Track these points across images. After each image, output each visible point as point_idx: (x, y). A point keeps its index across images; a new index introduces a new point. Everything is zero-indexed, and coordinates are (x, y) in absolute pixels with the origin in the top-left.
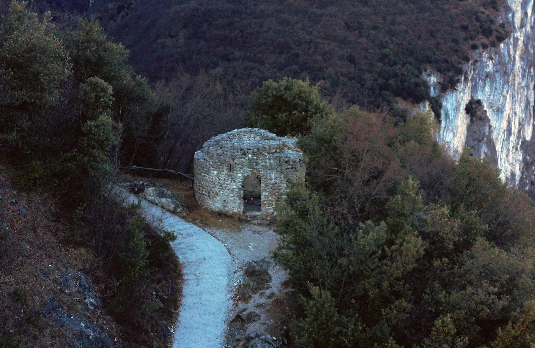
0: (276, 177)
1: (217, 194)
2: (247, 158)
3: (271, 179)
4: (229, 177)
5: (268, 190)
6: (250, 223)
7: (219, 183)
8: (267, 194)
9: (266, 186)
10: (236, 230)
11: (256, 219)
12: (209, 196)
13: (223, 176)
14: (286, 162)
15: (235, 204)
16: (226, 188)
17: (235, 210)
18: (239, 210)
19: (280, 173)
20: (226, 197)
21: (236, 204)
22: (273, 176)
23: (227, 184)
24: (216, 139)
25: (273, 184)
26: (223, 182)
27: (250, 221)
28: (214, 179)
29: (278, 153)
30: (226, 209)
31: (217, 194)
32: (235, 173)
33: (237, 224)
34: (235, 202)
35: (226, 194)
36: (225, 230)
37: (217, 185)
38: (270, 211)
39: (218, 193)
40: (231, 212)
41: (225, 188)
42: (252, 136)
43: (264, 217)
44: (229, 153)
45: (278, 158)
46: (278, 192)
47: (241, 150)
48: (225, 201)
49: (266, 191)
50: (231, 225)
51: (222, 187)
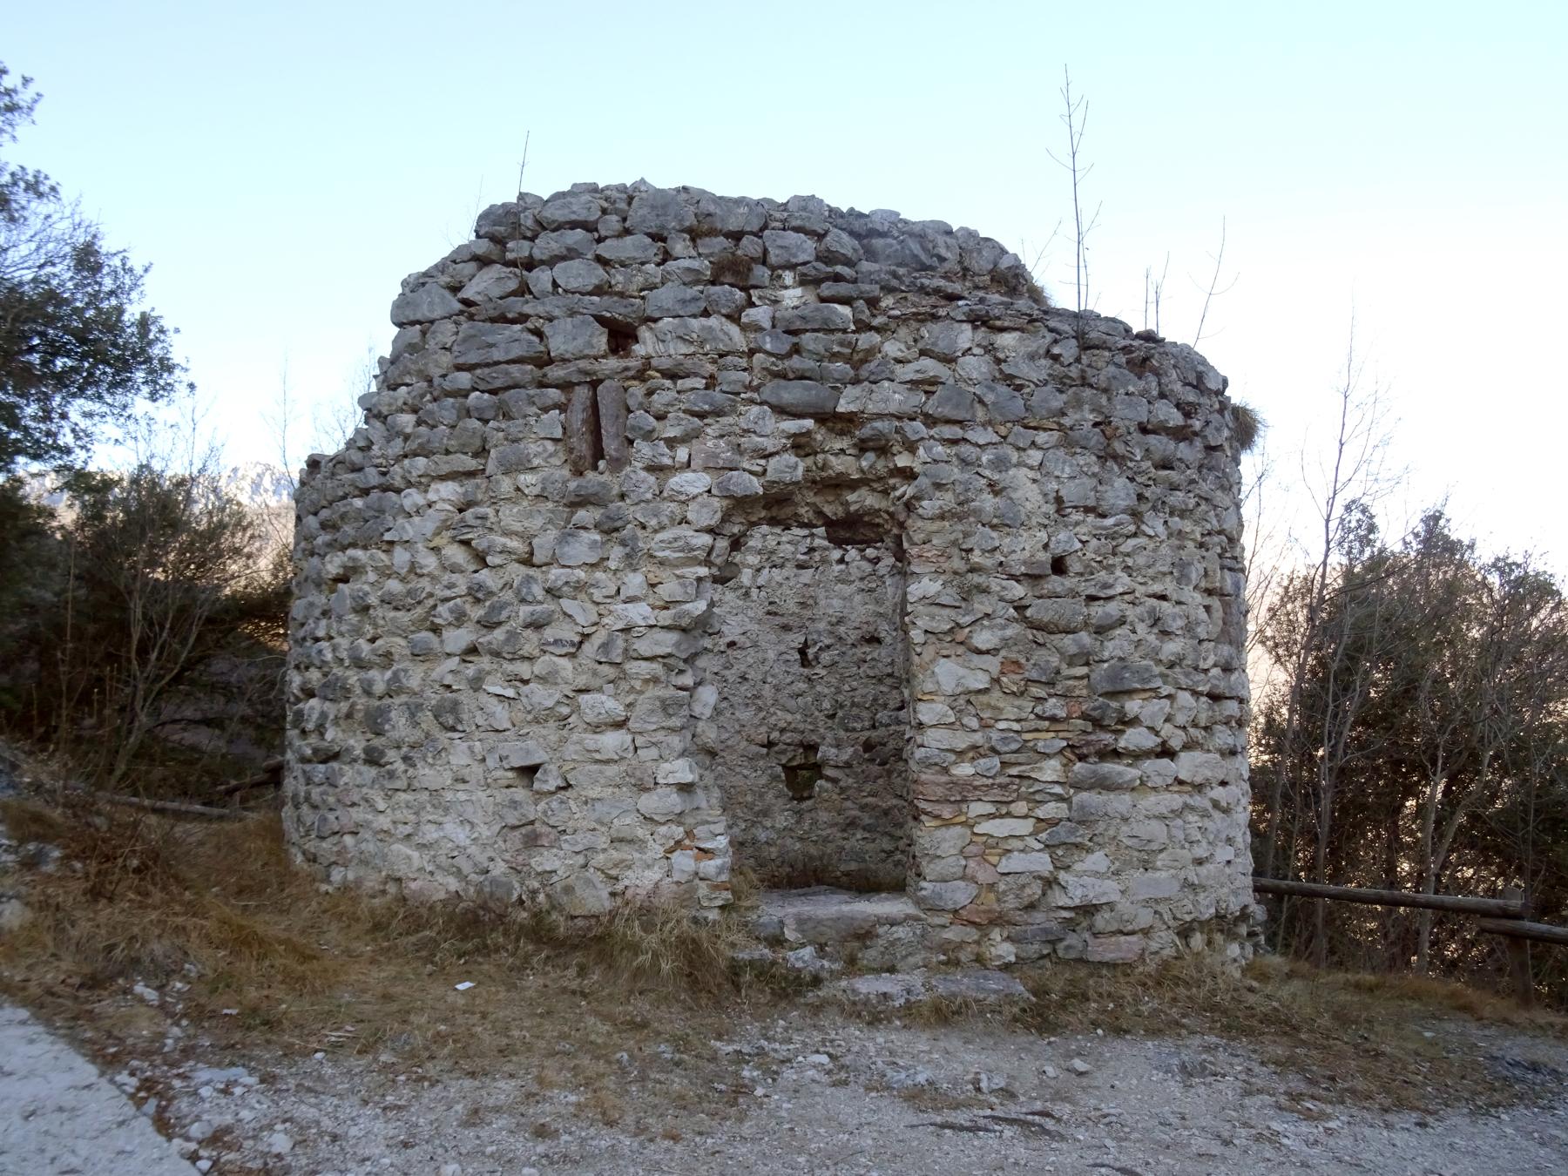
1: (449, 717)
4: (583, 515)
5: (983, 639)
6: (817, 1009)
7: (477, 594)
8: (981, 681)
9: (967, 594)
10: (678, 1083)
11: (870, 956)
12: (373, 758)
13: (510, 516)
15: (648, 803)
16: (549, 634)
17: (643, 878)
18: (684, 862)
19: (1088, 460)
20: (550, 732)
22: (1028, 493)
23: (552, 593)
26: (517, 572)
27: (816, 981)
28: (430, 562)
30: (545, 860)
31: (449, 717)
32: (638, 478)
33: (673, 1020)
35: (542, 696)
36: (504, 1090)
37: (460, 618)
38: (1015, 863)
39: (466, 698)
40: (595, 899)
41: (530, 642)
43: (951, 934)
44: (579, 274)
46: (1084, 657)
48: (529, 772)
49: (955, 639)
50: (598, 1029)
51: (499, 635)
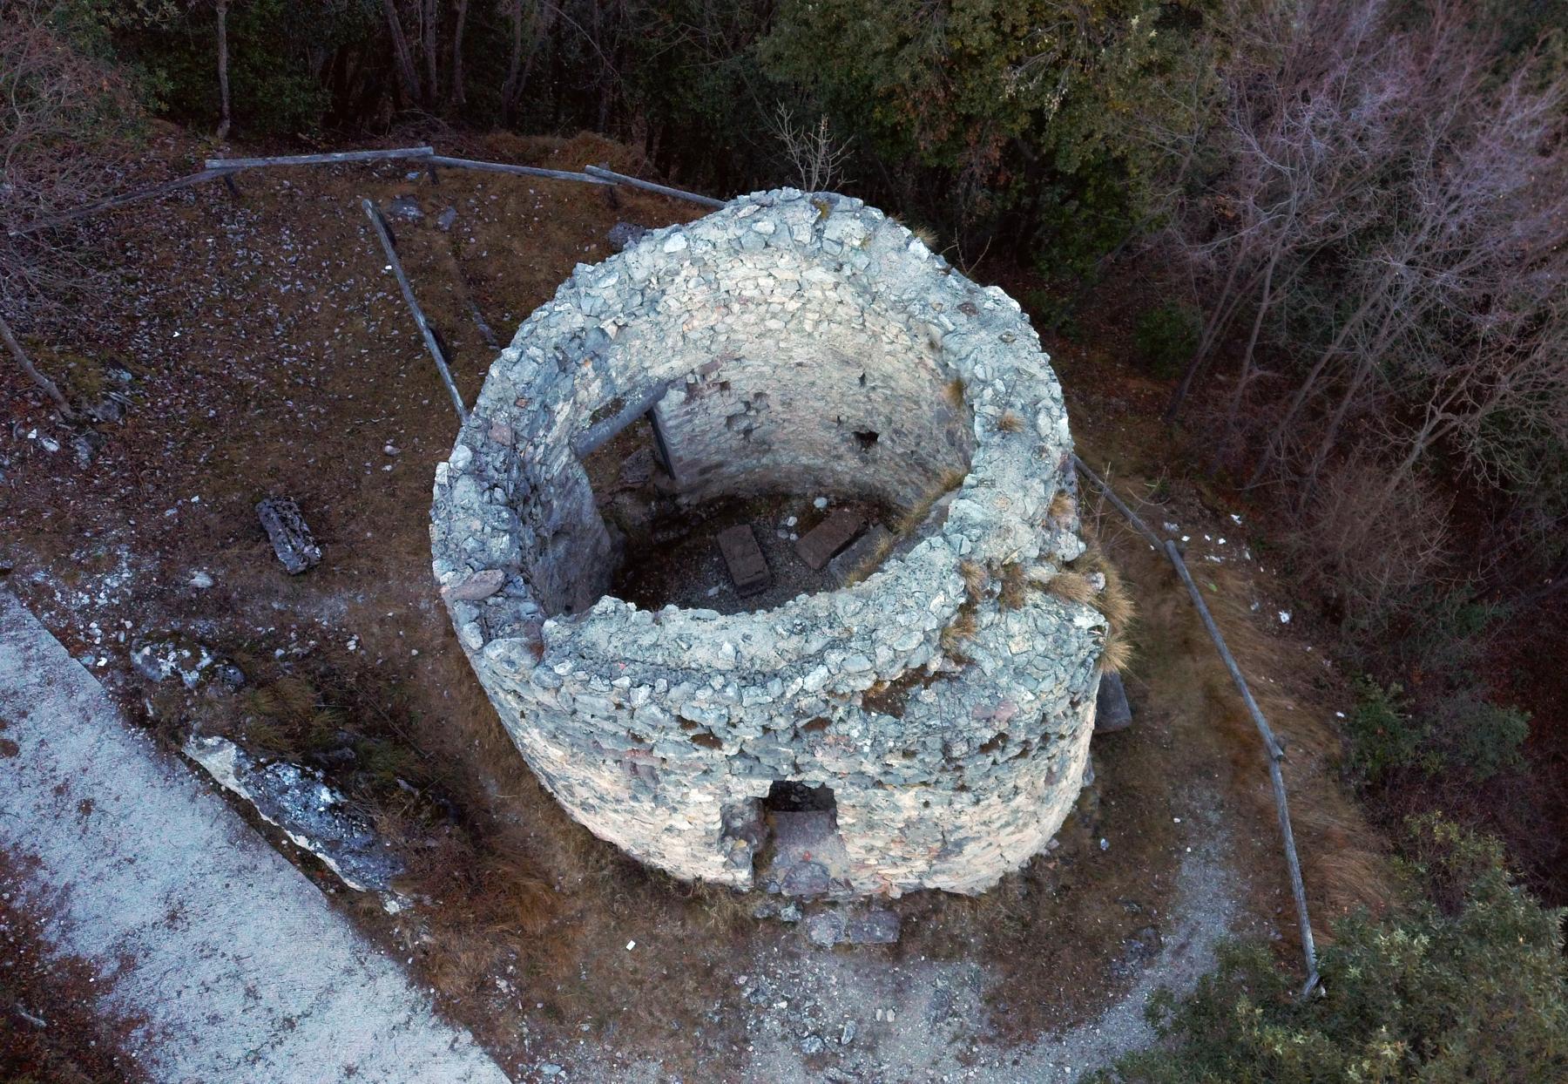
29: (939, 675)
45: (935, 742)
47: (685, 724)
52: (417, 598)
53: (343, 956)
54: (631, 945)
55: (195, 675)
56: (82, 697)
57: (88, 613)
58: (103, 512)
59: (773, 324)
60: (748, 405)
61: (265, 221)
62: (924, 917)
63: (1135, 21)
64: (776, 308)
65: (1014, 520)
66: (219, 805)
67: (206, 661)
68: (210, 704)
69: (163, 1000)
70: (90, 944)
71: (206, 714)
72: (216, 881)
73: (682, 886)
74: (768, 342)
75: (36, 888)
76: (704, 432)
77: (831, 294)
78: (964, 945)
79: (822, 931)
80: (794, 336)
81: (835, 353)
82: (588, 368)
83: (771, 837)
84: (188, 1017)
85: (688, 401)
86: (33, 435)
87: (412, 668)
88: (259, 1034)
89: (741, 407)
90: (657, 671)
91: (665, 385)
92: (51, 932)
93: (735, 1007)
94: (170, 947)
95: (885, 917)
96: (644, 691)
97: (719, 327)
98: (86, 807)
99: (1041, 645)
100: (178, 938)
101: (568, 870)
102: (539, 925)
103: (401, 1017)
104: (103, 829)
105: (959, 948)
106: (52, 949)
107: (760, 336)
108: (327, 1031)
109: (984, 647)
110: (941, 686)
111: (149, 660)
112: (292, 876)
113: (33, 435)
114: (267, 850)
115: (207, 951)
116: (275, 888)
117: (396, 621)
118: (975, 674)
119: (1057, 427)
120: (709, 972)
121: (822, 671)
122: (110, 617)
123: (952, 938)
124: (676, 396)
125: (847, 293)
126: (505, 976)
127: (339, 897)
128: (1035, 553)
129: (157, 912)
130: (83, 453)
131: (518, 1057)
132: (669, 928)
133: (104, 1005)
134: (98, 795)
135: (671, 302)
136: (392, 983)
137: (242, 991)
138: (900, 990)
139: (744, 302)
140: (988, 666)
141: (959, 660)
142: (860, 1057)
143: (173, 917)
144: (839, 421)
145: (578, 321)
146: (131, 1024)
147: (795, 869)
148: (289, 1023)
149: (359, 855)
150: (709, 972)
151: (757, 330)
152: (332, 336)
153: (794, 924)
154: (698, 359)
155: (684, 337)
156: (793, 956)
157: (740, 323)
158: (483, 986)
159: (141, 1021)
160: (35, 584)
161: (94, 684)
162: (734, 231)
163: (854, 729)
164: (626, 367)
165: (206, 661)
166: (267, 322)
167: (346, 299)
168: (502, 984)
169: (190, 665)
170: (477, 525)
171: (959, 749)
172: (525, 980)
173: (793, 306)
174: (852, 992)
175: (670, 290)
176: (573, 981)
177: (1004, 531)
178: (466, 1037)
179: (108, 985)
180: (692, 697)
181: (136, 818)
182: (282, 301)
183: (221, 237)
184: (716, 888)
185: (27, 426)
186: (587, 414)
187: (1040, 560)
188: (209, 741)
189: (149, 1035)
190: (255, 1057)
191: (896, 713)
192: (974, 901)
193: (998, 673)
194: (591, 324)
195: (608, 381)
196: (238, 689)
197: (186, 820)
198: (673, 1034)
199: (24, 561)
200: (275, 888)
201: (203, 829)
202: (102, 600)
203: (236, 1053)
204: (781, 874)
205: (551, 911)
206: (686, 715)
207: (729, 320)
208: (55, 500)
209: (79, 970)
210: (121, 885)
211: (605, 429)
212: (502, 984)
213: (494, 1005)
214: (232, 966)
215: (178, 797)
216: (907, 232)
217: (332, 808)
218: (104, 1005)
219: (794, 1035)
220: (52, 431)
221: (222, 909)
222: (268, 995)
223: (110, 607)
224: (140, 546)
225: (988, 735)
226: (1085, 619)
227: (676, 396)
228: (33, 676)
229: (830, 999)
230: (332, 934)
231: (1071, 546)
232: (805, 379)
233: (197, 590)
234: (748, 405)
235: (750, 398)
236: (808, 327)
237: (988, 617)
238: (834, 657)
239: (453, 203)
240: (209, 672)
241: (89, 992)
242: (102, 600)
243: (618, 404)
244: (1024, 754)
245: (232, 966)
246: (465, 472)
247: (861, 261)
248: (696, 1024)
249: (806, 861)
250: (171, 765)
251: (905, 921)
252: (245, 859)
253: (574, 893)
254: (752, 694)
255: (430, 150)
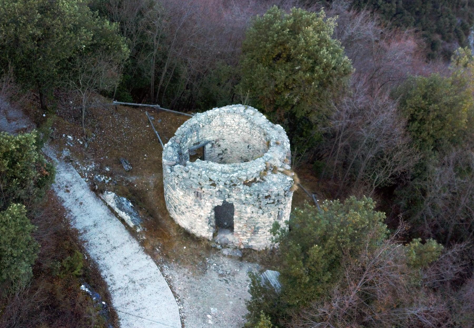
0: (253, 212)
2: (217, 189)
3: (246, 213)
9: (241, 219)
14: (266, 197)
19: (257, 209)
21: (204, 229)
24: (191, 124)
25: (249, 218)
29: (258, 182)
34: (203, 227)
40: (198, 235)
42: (236, 117)
45: (256, 193)
47: (211, 180)
52: (149, 180)
53: (127, 238)
54: (185, 248)
55: (108, 181)
56: (83, 185)
57: (85, 171)
58: (89, 156)
59: (232, 132)
60: (223, 151)
61: (122, 116)
62: (248, 254)
63: (313, 83)
64: (233, 128)
65: (277, 159)
66: (107, 208)
67: (110, 179)
68: (110, 186)
69: (91, 239)
70: (79, 227)
71: (109, 188)
72: (104, 221)
73: (197, 238)
74: (230, 136)
75: (70, 215)
76: (213, 157)
77: (245, 125)
78: (256, 261)
79: (225, 252)
80: (236, 135)
81: (243, 139)
82: (195, 133)
83: (217, 232)
84: (95, 243)
85: (212, 147)
86: (78, 140)
87: (146, 192)
88: (109, 249)
89: (221, 152)
90: (207, 169)
91: (209, 142)
92: (72, 223)
93: (205, 263)
94: (94, 230)
95: (240, 251)
96: (204, 172)
97: (221, 131)
98: (81, 204)
99: (279, 180)
100: (96, 229)
101: (173, 232)
102: (166, 241)
103: (137, 251)
104: (84, 208)
105: (254, 261)
106: (71, 226)
107: (229, 134)
108: (122, 250)
109: (268, 178)
110: (259, 184)
111: (99, 178)
112: (119, 222)
113: (78, 140)
114: (115, 217)
115: (101, 232)
116: (115, 224)
117: (144, 183)
118: (266, 183)
119: (288, 146)
120: (200, 256)
121: (237, 173)
122: (89, 173)
123: (253, 259)
124: (209, 145)
125: (248, 125)
126: (158, 248)
127: (127, 227)
128: (280, 166)
129: (92, 224)
130: (86, 146)
131: (159, 263)
132: (193, 246)
133: (80, 237)
134: (84, 202)
135: (213, 123)
136: (136, 245)
137: (106, 240)
138: (241, 267)
139: (227, 126)
140: (268, 182)
141: (263, 180)
142: (231, 277)
143: (95, 225)
144: (242, 158)
145: (196, 122)
146: (84, 242)
147: (221, 238)
148: (115, 248)
149: (135, 217)
150: (200, 256)
151: (228, 133)
152: (135, 136)
153: (220, 250)
154: (216, 138)
155: (214, 132)
156: (218, 256)
157: (225, 130)
158: (154, 249)
159: (87, 242)
160: (76, 164)
161: (85, 183)
162: (228, 109)
163: (241, 187)
164: (202, 136)
165: (110, 179)
166: (121, 132)
167: (138, 130)
168: (158, 250)
169: (107, 179)
170: (172, 154)
171: (261, 196)
172: (162, 250)
173: (237, 127)
174: (230, 265)
175: (214, 120)
176: (172, 251)
177: (274, 160)
178: (149, 257)
179: (81, 234)
180: (213, 174)
181: (90, 207)
182: (125, 129)
183: (113, 117)
184: (204, 239)
185: (78, 138)
186: (193, 143)
187: (281, 167)
188: (109, 192)
189: (88, 244)
190: (107, 252)
191: (250, 186)
192: (259, 253)
193: (270, 183)
194: (198, 123)
195: (198, 138)
196: (116, 185)
197: (100, 209)
198: (192, 265)
199: (76, 160)
200: (115, 224)
201: (103, 211)
202: (88, 169)
203: (104, 251)
204: (218, 239)
205: (169, 239)
206: (211, 178)
207: (223, 130)
208: (81, 151)
209: (76, 231)
210: (86, 218)
211: (195, 147)
212: (158, 250)
213: (155, 253)
214: (105, 236)
215: (98, 205)
216: (262, 114)
217: (132, 207)
218: (80, 237)
219: (217, 270)
220: (82, 140)
221: (105, 226)
222: (111, 242)
223: (90, 171)
224: (96, 162)
225: (267, 194)
226: (289, 179)
227: (209, 145)
228: (74, 180)
229: (226, 266)
230: (125, 234)
231: (288, 167)
232: (236, 146)
233: (107, 171)
234: (223, 151)
235: (224, 150)
236: (239, 133)
237: (269, 173)
238: (239, 172)
239: (161, 118)
240: (110, 181)
241: (78, 235)
242: (88, 169)
243: (199, 143)
244: (273, 203)
245: (105, 236)
246: (170, 146)
247: (252, 117)
248: (197, 264)
249: (224, 237)
250: (98, 199)
251: (243, 254)
252: (110, 218)
253: (174, 237)
254: (223, 175)
255: (159, 106)
